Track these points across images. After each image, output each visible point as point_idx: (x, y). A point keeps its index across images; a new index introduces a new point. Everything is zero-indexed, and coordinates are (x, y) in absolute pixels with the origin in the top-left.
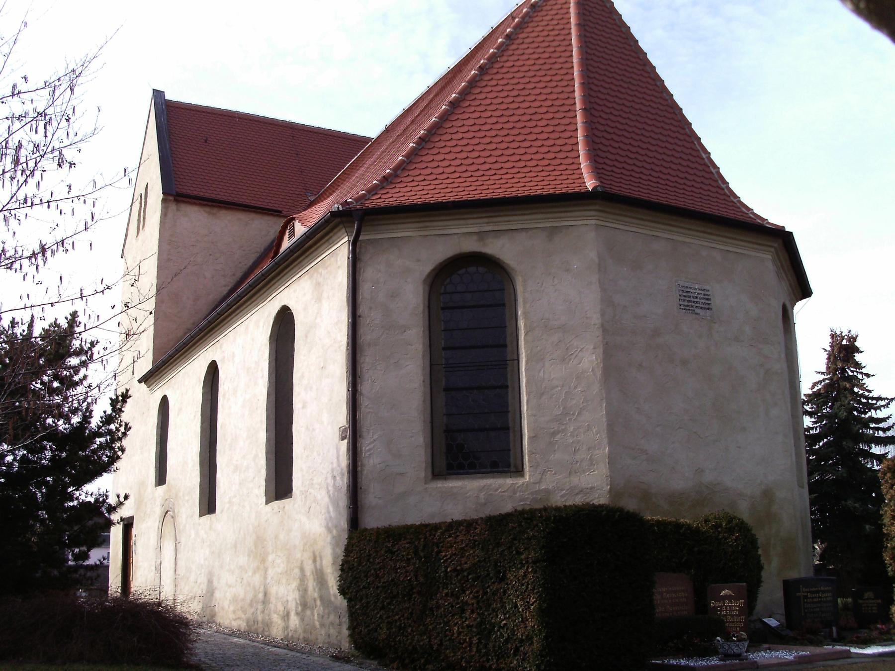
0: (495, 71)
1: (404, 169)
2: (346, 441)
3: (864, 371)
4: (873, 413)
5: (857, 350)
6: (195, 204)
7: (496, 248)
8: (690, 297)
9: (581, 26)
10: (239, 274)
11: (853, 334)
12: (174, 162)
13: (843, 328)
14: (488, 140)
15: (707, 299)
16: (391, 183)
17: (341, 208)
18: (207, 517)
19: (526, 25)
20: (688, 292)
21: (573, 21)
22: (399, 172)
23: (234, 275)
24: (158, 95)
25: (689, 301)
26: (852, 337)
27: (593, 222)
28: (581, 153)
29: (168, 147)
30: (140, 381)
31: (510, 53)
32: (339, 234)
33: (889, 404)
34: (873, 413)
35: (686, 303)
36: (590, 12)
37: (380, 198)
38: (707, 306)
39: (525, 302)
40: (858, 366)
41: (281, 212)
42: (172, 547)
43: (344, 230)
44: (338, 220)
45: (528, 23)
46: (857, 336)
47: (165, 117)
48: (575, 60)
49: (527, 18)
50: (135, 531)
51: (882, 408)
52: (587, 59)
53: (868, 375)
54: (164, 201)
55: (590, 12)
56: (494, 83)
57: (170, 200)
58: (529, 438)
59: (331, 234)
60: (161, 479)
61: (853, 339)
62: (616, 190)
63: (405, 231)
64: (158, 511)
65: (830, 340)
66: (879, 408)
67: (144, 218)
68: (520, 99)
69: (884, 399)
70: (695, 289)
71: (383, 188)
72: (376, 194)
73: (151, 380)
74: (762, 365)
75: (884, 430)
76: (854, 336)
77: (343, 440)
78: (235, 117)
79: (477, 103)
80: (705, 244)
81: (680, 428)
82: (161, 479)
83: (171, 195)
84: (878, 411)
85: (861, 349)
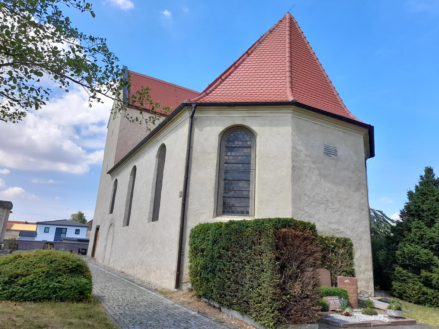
2: (182, 198)
7: (248, 123)
8: (328, 149)
15: (336, 151)
17: (187, 102)
18: (126, 227)
20: (328, 147)
25: (328, 151)
27: (291, 115)
30: (108, 173)
35: (327, 152)
38: (336, 154)
39: (260, 146)
42: (112, 239)
43: (188, 112)
50: (100, 231)
58: (258, 202)
59: (182, 114)
60: (111, 212)
63: (212, 114)
64: (109, 224)
70: (331, 146)
73: (112, 173)
74: (357, 181)
77: (180, 197)
81: (322, 204)
82: (111, 212)
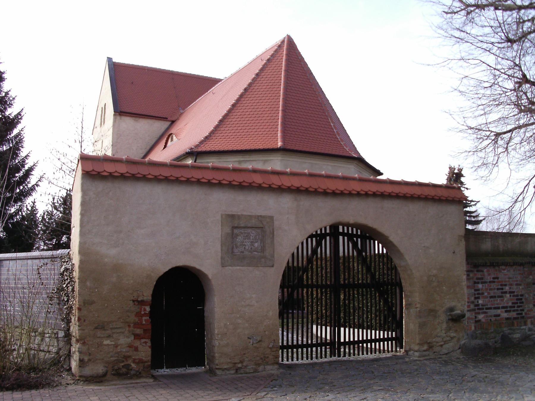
0: (251, 90)
1: (213, 133)
3: (465, 186)
4: (468, 209)
5: (462, 176)
6: (128, 116)
9: (286, 71)
10: (148, 148)
11: (461, 167)
12: (119, 95)
13: (455, 165)
14: (245, 122)
16: (209, 139)
17: (189, 151)
19: (265, 69)
21: (283, 68)
22: (212, 134)
23: (146, 148)
24: (109, 60)
26: (460, 169)
28: (279, 129)
29: (115, 87)
31: (257, 82)
32: (189, 159)
33: (476, 204)
34: (468, 209)
36: (291, 62)
37: (204, 146)
40: (462, 183)
41: (167, 118)
44: (187, 155)
45: (266, 68)
46: (463, 169)
47: (113, 72)
48: (282, 87)
49: (265, 66)
51: (473, 206)
52: (287, 86)
53: (467, 189)
54: (114, 115)
55: (291, 62)
56: (250, 96)
57: (117, 115)
61: (460, 170)
62: (289, 147)
65: (449, 170)
66: (471, 206)
67: (104, 119)
68: (259, 104)
69: (474, 201)
71: (205, 141)
72: (203, 144)
75: (474, 217)
76: (461, 168)
78: (145, 70)
79: (243, 105)
80: (325, 163)
83: (118, 112)
84: (471, 207)
85: (464, 175)
